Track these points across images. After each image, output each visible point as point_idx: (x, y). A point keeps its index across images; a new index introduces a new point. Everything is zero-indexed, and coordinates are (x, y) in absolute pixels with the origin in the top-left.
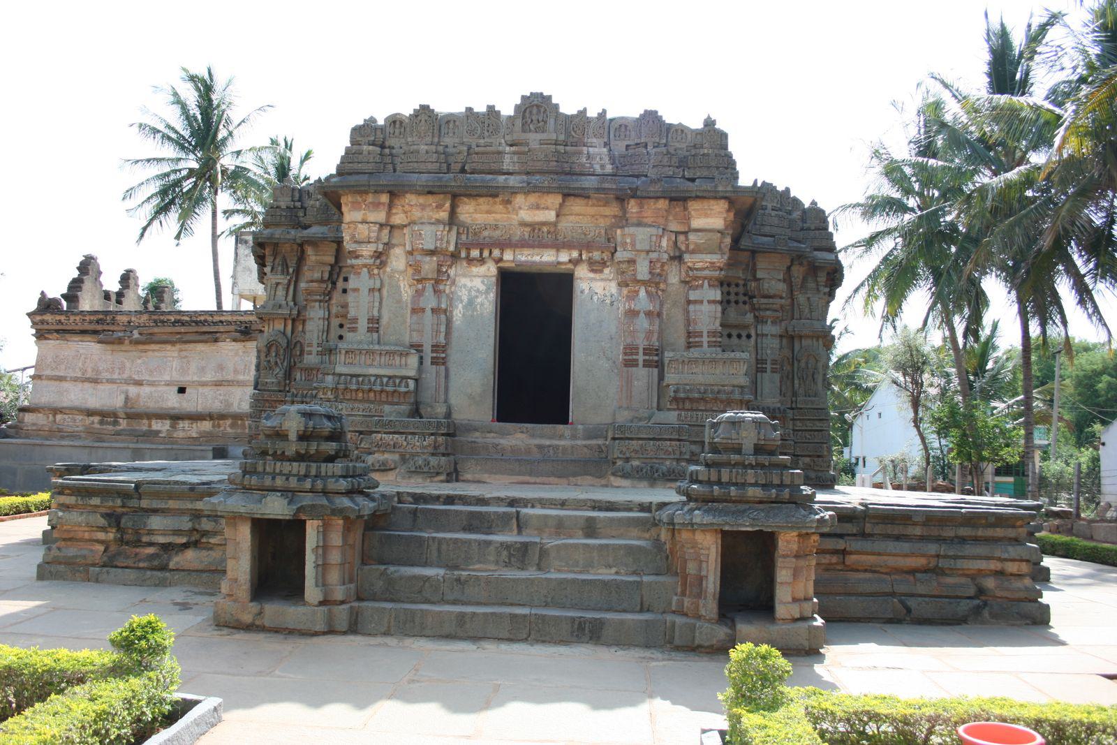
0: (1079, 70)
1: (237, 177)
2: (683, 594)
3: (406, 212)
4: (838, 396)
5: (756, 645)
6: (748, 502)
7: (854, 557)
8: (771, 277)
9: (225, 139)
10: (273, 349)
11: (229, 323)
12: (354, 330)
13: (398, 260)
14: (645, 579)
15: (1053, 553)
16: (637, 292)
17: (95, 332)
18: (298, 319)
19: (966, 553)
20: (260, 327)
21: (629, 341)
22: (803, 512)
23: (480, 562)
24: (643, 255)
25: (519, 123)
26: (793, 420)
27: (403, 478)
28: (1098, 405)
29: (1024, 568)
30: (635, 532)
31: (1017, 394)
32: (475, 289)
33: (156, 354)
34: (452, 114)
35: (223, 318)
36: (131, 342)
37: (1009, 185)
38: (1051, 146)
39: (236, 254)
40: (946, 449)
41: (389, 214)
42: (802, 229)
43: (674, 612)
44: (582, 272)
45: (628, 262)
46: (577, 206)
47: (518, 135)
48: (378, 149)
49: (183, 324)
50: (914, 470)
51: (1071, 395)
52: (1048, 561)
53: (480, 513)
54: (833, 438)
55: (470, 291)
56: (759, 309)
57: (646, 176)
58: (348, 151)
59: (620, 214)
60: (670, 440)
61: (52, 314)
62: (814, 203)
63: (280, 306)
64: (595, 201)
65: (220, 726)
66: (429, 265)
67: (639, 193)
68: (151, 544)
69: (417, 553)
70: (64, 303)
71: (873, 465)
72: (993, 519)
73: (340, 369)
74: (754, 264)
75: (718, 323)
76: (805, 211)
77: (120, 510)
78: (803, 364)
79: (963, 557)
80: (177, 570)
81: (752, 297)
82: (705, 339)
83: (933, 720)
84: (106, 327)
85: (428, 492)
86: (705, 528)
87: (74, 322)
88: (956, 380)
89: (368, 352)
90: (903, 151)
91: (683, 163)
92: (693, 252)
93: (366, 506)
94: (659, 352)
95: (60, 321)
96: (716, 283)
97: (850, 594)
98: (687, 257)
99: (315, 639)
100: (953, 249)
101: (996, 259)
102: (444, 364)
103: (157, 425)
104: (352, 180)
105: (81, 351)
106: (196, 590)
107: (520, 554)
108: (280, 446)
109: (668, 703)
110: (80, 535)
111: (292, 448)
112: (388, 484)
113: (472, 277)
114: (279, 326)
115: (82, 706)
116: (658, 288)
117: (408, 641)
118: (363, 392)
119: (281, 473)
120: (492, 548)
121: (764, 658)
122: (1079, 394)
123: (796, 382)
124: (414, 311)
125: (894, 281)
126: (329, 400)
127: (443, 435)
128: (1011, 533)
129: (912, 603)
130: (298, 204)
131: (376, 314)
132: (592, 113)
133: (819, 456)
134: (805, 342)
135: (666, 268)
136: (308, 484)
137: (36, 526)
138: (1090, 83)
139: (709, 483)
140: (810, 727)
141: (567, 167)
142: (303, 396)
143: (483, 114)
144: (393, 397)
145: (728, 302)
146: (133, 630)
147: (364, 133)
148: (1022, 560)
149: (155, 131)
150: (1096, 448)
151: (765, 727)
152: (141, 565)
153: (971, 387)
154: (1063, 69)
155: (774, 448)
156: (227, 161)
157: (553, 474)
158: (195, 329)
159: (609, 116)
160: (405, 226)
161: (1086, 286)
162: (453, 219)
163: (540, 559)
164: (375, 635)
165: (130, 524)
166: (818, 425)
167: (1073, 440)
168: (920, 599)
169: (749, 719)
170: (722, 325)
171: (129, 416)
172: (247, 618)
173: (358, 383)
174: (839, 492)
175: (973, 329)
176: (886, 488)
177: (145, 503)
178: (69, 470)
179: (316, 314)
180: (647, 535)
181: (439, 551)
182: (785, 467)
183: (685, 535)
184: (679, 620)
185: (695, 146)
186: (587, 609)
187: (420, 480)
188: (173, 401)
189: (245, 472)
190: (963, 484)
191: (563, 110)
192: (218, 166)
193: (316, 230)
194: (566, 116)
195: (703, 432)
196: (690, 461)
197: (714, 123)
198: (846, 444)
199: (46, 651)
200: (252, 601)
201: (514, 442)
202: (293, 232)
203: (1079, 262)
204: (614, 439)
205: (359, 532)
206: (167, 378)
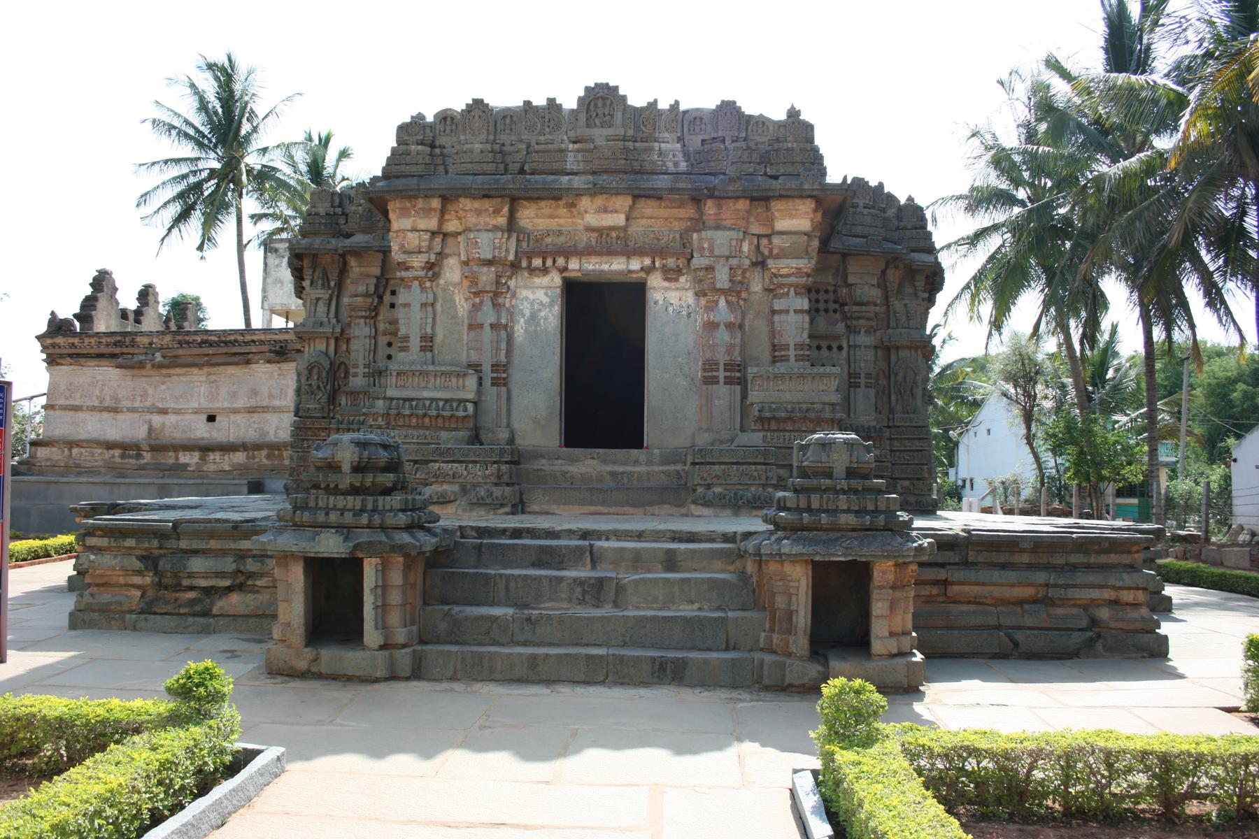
0: (1205, 44)
1: (264, 176)
2: (772, 630)
3: (460, 219)
4: (942, 411)
5: (850, 680)
6: (840, 530)
7: (956, 588)
8: (864, 282)
9: (249, 134)
10: (315, 371)
11: (262, 342)
12: (405, 349)
13: (452, 272)
14: (730, 614)
15: (1178, 582)
16: (717, 302)
17: (113, 356)
18: (342, 338)
19: (1078, 581)
20: (299, 347)
21: (708, 356)
22: (899, 539)
23: (552, 600)
24: (723, 261)
25: (582, 118)
26: (891, 439)
27: (465, 510)
28: (1232, 417)
29: (1141, 597)
30: (719, 564)
31: (1142, 406)
32: (538, 302)
33: (182, 378)
34: (508, 109)
35: (255, 338)
36: (153, 366)
37: (1127, 174)
38: (1176, 129)
39: (265, 264)
40: (1062, 469)
41: (441, 221)
42: (898, 229)
43: (762, 650)
44: (655, 281)
45: (706, 269)
46: (648, 208)
47: (582, 131)
48: (428, 149)
49: (211, 344)
50: (1027, 492)
51: (1202, 406)
52: (1170, 590)
53: (551, 547)
54: (937, 458)
55: (532, 304)
56: (852, 318)
57: (724, 174)
58: (394, 151)
59: (696, 216)
60: (755, 464)
61: (64, 336)
62: (910, 199)
63: (321, 324)
64: (668, 203)
65: (283, 777)
66: (487, 276)
67: (716, 193)
68: (192, 588)
69: (483, 592)
70: (77, 324)
71: (981, 488)
72: (1107, 545)
73: (391, 393)
74: (845, 269)
75: (805, 335)
76: (900, 209)
77: (157, 552)
78: (900, 378)
79: (1074, 586)
80: (221, 615)
81: (843, 305)
82: (792, 353)
83: (1036, 755)
84: (125, 350)
85: (492, 525)
86: (794, 559)
87: (89, 345)
88: (1072, 393)
89: (422, 373)
90: (1011, 139)
91: (765, 159)
92: (777, 257)
93: (428, 542)
94: (741, 367)
95: (73, 344)
96: (803, 291)
97: (952, 628)
98: (771, 263)
99: (377, 686)
100: (1068, 244)
101: (1115, 257)
102: (505, 385)
103: (184, 458)
104: (400, 183)
105: (98, 377)
106: (243, 636)
107: (595, 591)
108: (332, 478)
109: (757, 745)
110: (114, 580)
111: (346, 481)
112: (451, 518)
113: (534, 288)
114: (321, 346)
115: (144, 755)
116: (739, 298)
117: (477, 686)
118: (417, 417)
119: (335, 508)
120: (564, 584)
121: (858, 692)
122: (1212, 405)
123: (893, 397)
124: (471, 327)
125: (1003, 282)
126: (380, 427)
127: (506, 462)
128: (1125, 559)
129: (1019, 636)
130: (339, 210)
131: (429, 330)
132: (663, 105)
133: (919, 479)
134: (902, 354)
135: (747, 275)
136: (364, 520)
137: (60, 572)
138: (1217, 58)
139: (798, 510)
140: (906, 764)
141: (636, 166)
142: (349, 423)
143: (543, 108)
144: (451, 422)
145: (817, 310)
146: (190, 677)
147: (411, 132)
148: (1138, 589)
149: (172, 127)
150: (1228, 466)
151: (859, 763)
152: (182, 611)
153: (1090, 399)
154: (1187, 42)
155: (867, 471)
156: (252, 160)
157: (628, 504)
158: (225, 350)
159: (682, 107)
160: (460, 234)
161: (1215, 285)
162: (511, 225)
163: (617, 596)
164: (440, 680)
165: (168, 567)
166: (917, 445)
167: (1204, 456)
168: (1028, 632)
169: (842, 756)
170: (810, 337)
171: (154, 449)
172: (302, 665)
173: (411, 407)
174: (941, 518)
175: (1090, 336)
176: (996, 513)
177: (184, 544)
178: (94, 510)
179: (361, 330)
180: (732, 568)
181: (507, 588)
182: (879, 491)
183: (773, 567)
184: (768, 658)
185: (777, 140)
186: (668, 648)
187: (483, 513)
188: (202, 431)
189: (296, 508)
190: (1082, 508)
191: (630, 102)
192: (243, 166)
193: (359, 239)
194: (635, 109)
195: (791, 454)
196: (777, 487)
197: (798, 113)
198: (952, 464)
199: (96, 702)
200: (307, 646)
201: (584, 470)
202: (333, 241)
203: (1206, 257)
204: (694, 464)
205: (420, 570)
206: (194, 405)
